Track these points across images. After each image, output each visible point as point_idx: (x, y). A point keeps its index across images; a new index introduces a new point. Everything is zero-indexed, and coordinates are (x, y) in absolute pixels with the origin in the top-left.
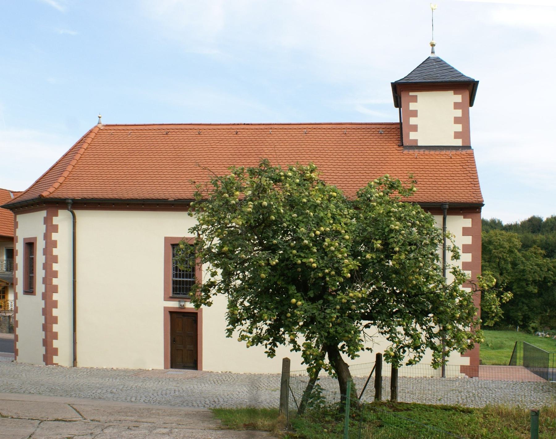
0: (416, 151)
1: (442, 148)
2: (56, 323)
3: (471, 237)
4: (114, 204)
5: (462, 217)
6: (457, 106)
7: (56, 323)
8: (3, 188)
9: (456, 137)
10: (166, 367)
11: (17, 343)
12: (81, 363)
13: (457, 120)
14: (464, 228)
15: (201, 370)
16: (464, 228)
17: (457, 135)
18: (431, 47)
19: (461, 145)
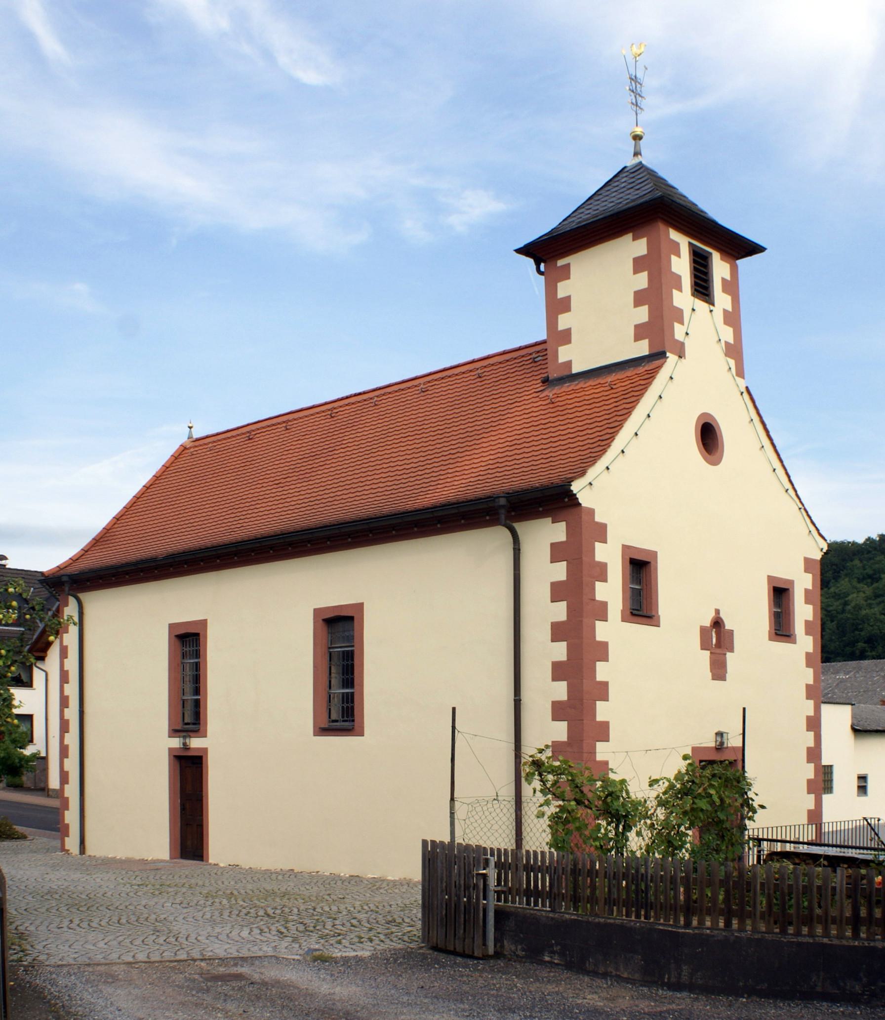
0: (573, 386)
1: (613, 368)
2: (605, 698)
3: (565, 563)
4: (127, 574)
5: (549, 519)
6: (639, 264)
7: (605, 698)
8: (19, 568)
9: (638, 338)
10: (172, 857)
11: (66, 812)
12: (91, 850)
13: (640, 298)
14: (552, 545)
15: (207, 861)
16: (552, 545)
17: (640, 332)
18: (633, 142)
19: (647, 353)
